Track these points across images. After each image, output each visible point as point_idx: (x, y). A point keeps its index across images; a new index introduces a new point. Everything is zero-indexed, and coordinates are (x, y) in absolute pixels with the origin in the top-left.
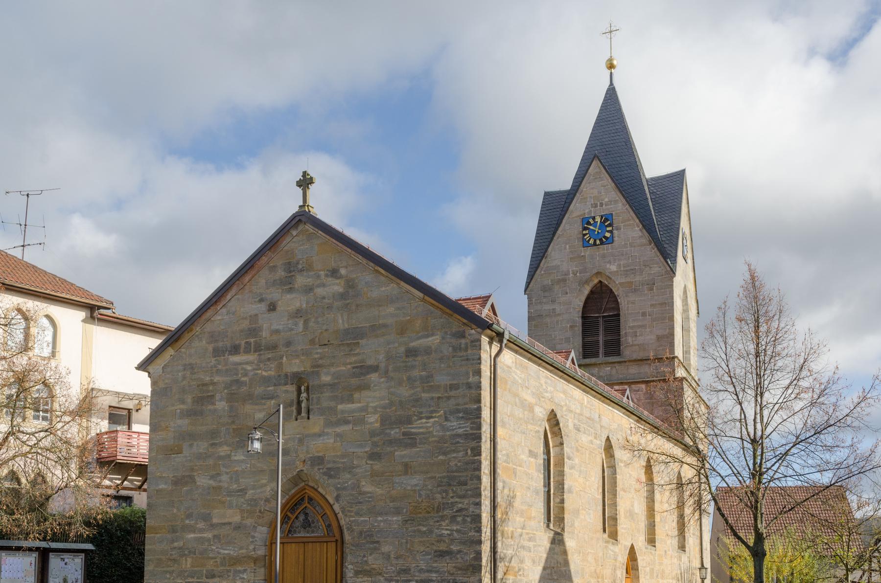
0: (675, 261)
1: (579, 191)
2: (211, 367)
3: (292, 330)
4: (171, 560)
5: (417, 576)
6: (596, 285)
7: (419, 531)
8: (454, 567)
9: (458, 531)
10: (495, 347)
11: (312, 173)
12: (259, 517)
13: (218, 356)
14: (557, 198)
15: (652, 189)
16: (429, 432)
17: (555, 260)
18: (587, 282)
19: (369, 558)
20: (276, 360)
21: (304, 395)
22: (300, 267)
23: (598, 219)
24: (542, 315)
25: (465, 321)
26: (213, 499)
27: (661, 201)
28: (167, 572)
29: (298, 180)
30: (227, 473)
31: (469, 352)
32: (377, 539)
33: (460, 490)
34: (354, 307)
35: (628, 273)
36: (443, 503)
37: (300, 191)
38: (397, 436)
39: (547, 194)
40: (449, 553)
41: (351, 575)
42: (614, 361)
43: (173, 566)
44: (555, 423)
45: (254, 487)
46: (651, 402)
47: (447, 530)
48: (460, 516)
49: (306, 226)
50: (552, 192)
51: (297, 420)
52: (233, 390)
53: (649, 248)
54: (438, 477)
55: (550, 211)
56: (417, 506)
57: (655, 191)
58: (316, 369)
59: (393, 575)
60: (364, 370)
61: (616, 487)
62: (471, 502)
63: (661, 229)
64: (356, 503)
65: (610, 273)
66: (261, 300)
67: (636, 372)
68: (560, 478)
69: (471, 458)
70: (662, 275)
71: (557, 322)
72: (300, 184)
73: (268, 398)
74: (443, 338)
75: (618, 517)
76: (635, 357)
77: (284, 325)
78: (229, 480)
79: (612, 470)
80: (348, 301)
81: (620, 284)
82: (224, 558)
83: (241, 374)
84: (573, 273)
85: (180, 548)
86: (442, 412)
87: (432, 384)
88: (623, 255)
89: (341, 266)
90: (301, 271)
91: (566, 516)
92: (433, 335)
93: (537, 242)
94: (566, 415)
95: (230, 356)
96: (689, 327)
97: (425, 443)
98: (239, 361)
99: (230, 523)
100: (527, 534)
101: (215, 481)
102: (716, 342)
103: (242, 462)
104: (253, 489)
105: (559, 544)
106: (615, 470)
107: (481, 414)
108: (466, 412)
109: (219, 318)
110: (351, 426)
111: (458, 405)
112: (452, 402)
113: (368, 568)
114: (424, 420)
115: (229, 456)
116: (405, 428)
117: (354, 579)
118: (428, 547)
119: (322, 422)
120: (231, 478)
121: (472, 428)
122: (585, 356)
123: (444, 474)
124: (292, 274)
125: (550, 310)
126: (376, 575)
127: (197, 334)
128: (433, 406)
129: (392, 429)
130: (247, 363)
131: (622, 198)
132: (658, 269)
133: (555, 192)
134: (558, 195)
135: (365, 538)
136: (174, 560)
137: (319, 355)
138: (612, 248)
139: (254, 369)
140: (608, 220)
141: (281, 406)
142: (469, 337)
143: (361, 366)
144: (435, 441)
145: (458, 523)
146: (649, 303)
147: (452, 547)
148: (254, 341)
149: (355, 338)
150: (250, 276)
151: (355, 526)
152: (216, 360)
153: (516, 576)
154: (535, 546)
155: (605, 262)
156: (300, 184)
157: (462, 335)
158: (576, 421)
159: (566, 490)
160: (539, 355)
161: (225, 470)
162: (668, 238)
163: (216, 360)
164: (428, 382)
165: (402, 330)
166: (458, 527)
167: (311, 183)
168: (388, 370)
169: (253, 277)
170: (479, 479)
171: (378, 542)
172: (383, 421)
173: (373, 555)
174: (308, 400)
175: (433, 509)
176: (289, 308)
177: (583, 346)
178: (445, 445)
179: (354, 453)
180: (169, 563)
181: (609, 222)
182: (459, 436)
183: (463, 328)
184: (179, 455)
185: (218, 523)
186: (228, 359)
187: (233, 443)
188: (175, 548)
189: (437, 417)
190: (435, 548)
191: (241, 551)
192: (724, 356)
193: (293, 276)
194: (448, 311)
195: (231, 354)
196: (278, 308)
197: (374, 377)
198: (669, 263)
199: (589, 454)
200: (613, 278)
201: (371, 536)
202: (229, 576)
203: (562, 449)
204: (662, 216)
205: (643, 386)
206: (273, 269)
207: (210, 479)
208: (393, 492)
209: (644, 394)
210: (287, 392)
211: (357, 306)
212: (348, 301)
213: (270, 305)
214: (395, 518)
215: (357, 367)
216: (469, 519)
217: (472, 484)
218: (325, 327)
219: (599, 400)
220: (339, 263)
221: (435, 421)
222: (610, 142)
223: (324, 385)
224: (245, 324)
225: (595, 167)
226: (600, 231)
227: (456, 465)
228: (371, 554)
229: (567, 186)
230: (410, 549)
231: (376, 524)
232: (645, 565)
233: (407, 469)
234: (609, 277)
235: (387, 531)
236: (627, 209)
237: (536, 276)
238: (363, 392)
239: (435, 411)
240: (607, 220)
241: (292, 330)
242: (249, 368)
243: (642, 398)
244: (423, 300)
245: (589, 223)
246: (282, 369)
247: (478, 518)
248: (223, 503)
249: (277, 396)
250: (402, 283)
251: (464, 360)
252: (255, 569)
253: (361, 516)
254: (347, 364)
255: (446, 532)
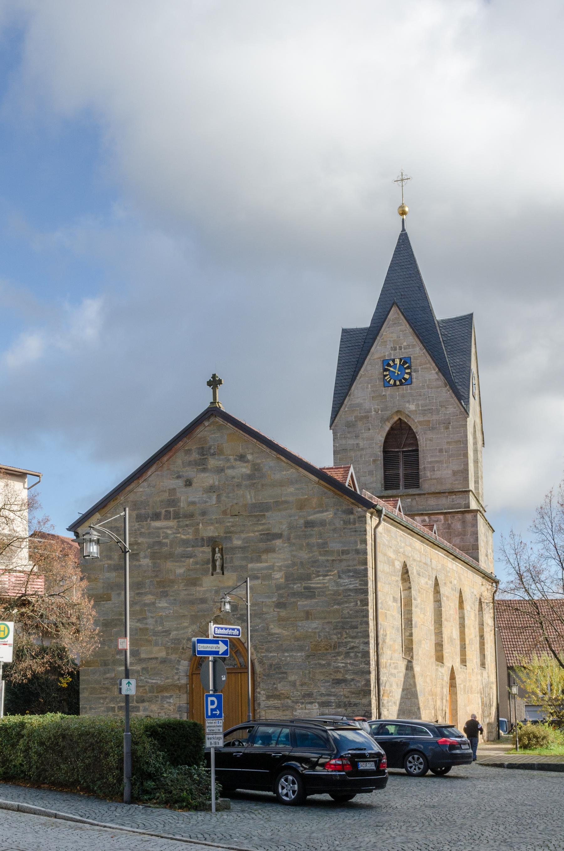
0: (467, 403)
1: (380, 334)
2: (135, 530)
3: (206, 502)
4: (104, 688)
5: (319, 699)
6: (395, 423)
7: (320, 664)
8: (349, 692)
9: (351, 664)
10: (375, 520)
11: (219, 376)
12: (182, 653)
13: (141, 522)
14: (354, 336)
15: (443, 331)
16: (325, 587)
17: (358, 398)
18: (388, 419)
19: (278, 685)
20: (193, 526)
21: (218, 555)
22: (212, 451)
23: (397, 361)
24: (346, 450)
25: (353, 501)
26: (140, 639)
27: (452, 344)
28: (100, 698)
29: (208, 380)
30: (152, 617)
31: (357, 525)
32: (284, 671)
33: (353, 632)
34: (260, 486)
35: (426, 412)
36: (339, 643)
37: (210, 390)
38: (299, 589)
39: (344, 331)
40: (344, 681)
41: (264, 699)
42: (414, 493)
43: (106, 693)
44: (405, 571)
45: (177, 629)
46: (448, 533)
47: (342, 663)
48: (353, 652)
49: (217, 419)
50: (349, 329)
51: (212, 575)
52: (156, 550)
53: (444, 390)
54: (334, 622)
55: (349, 348)
56: (317, 645)
57: (446, 333)
58: (229, 535)
59: (299, 699)
60: (270, 536)
61: (442, 618)
62: (361, 641)
63: (454, 371)
64: (266, 642)
65: (410, 412)
66: (179, 477)
67: (434, 504)
68: (409, 616)
69: (360, 607)
70: (457, 416)
71: (361, 456)
72: (209, 384)
73: (188, 557)
74: (335, 514)
75: (443, 643)
76: (433, 490)
77: (199, 498)
78: (154, 623)
79: (438, 603)
80: (254, 481)
81: (419, 422)
82: (152, 686)
83: (163, 537)
84: (375, 411)
85: (112, 679)
86: (336, 571)
87: (327, 549)
88: (421, 395)
89: (248, 452)
90: (213, 454)
91: (414, 646)
92: (327, 511)
93: (338, 378)
94: (412, 564)
95: (152, 522)
96: (478, 459)
97: (322, 596)
98: (159, 526)
99: (157, 658)
100: (394, 663)
101: (141, 623)
102: (545, 521)
103: (166, 608)
104: (176, 630)
105: (411, 670)
106: (441, 604)
107: (367, 574)
108: (356, 571)
109: (141, 490)
110: (260, 581)
111: (349, 566)
112: (344, 564)
113: (278, 693)
114: (321, 578)
115: (154, 603)
116: (305, 583)
117: (265, 702)
118: (327, 676)
119: (235, 578)
120: (156, 621)
121: (361, 585)
122: (387, 487)
123: (339, 620)
124: (205, 457)
125: (354, 444)
126: (284, 698)
127: (121, 502)
128: (328, 567)
129: (294, 584)
130: (167, 528)
131: (419, 343)
132: (452, 410)
133: (352, 329)
134: (354, 333)
135: (275, 669)
136: (106, 688)
137: (230, 524)
138: (411, 389)
139: (174, 533)
140: (407, 363)
141: (248, 578)
142: (357, 514)
143: (268, 533)
144: (331, 594)
145: (351, 658)
146: (445, 441)
147: (346, 676)
148: (173, 510)
149: (262, 511)
150: (167, 457)
151: (266, 660)
152: (139, 525)
153: (388, 697)
154: (398, 672)
155: (405, 402)
156: (209, 384)
157: (351, 513)
158: (418, 568)
159: (413, 626)
160: (393, 517)
161: (150, 615)
162: (461, 380)
163: (139, 525)
164: (324, 548)
165: (301, 506)
166: (351, 661)
167: (219, 384)
168: (290, 538)
169: (170, 457)
170: (367, 623)
171: (285, 673)
172: (288, 577)
173: (282, 683)
174: (222, 559)
175: (331, 647)
176: (204, 485)
177: (384, 478)
178: (339, 597)
179: (263, 602)
180: (102, 691)
181: (408, 365)
182: (350, 590)
183: (351, 506)
184: (109, 602)
185: (145, 658)
186: (150, 523)
187: (157, 592)
188: (107, 678)
189: (332, 575)
190: (332, 677)
191: (167, 681)
192: (551, 533)
193: (206, 458)
194: (339, 492)
195: (152, 519)
196: (194, 484)
197: (278, 542)
198: (463, 404)
199: (426, 594)
200: (412, 417)
201: (280, 668)
202: (157, 701)
203: (410, 592)
204: (455, 358)
205: (442, 517)
206: (189, 452)
207: (137, 622)
208: (296, 633)
209: (443, 524)
210: (203, 552)
211: (263, 485)
212: (254, 481)
213: (186, 481)
214: (299, 654)
215: (264, 534)
216: (360, 655)
217: (361, 627)
218: (235, 501)
219: (430, 546)
220: (246, 450)
221: (330, 579)
222: (404, 286)
223: (236, 548)
224: (165, 496)
225: (394, 313)
226: (399, 373)
227: (348, 613)
228: (280, 682)
229: (366, 323)
230: (312, 678)
231: (283, 659)
232: (460, 683)
233: (308, 615)
234: (409, 416)
235: (293, 664)
236: (424, 353)
237: (340, 412)
238: (269, 554)
239: (330, 571)
240: (406, 362)
241: (206, 502)
242: (169, 532)
243: (441, 528)
244: (318, 483)
245: (389, 365)
246: (199, 533)
247: (366, 654)
248: (150, 641)
249: (195, 555)
250: (301, 469)
251: (353, 531)
252: (180, 695)
253: (271, 652)
254: (255, 532)
255: (342, 665)
